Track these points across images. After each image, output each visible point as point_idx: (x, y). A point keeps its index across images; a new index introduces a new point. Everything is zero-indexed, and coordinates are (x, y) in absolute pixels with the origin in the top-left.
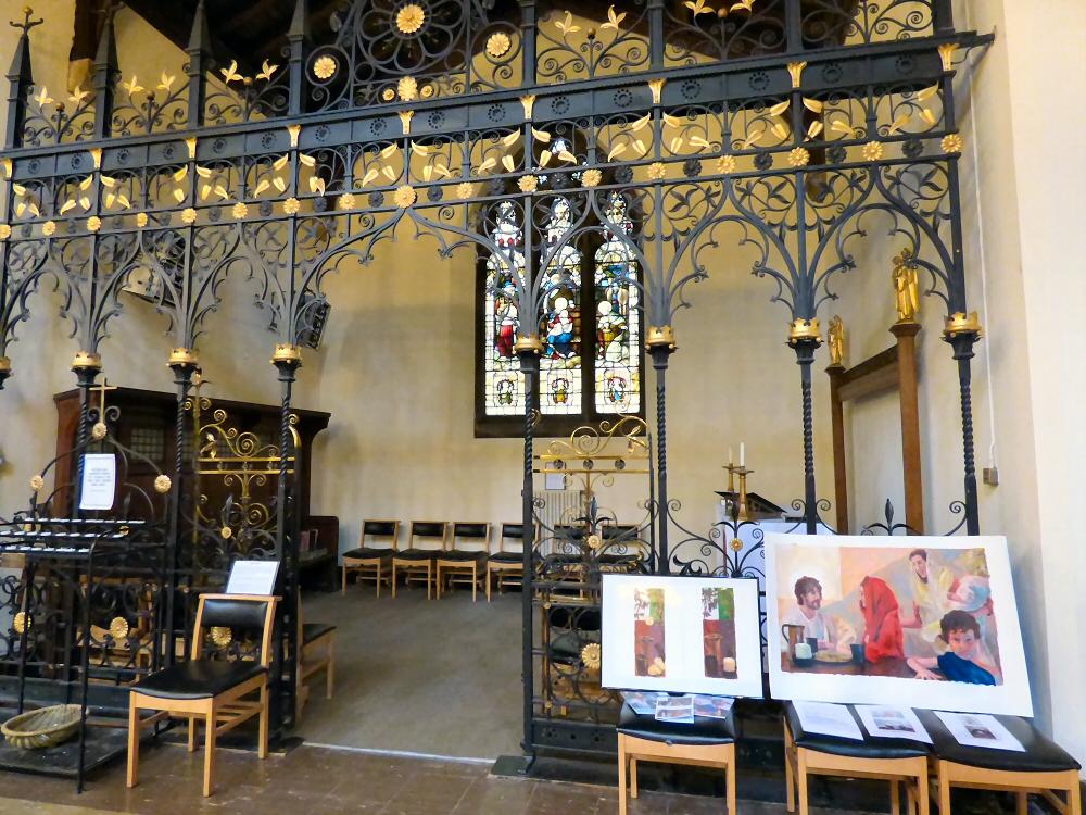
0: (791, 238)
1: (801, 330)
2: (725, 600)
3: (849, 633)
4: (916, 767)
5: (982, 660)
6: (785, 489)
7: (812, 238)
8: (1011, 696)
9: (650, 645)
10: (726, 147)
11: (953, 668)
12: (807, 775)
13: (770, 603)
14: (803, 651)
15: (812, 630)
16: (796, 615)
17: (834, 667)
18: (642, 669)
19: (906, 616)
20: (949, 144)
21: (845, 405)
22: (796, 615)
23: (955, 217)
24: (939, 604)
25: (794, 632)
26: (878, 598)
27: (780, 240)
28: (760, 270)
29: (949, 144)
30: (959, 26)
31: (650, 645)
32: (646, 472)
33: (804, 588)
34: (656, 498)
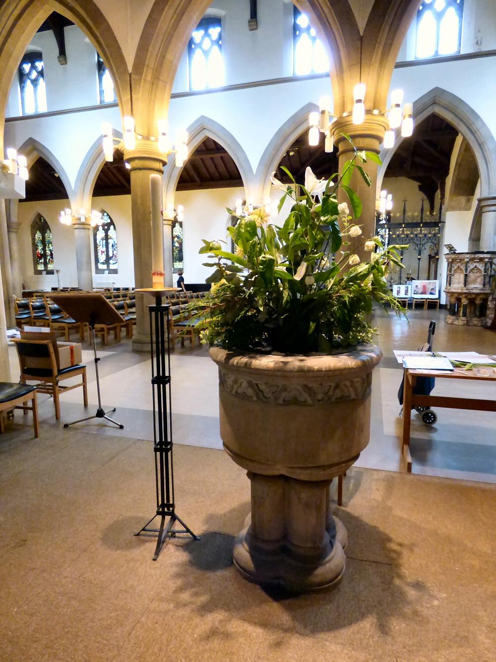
0: (419, 246)
1: (419, 257)
2: (407, 287)
3: (420, 291)
4: (425, 300)
5: (434, 293)
6: (415, 276)
7: (421, 246)
8: (436, 296)
9: (398, 292)
10: (412, 233)
11: (431, 294)
12: (68, 198)
13: (412, 288)
14: (416, 292)
15: (417, 290)
16: (415, 289)
17: (419, 294)
18: (398, 295)
19: (427, 288)
20: (439, 235)
21: (431, 262)
22: (415, 289)
23: (438, 244)
24: (431, 287)
25: (415, 291)
26: (424, 287)
27: (418, 246)
28: (415, 249)
29: (439, 235)
30: (442, 221)
31: (398, 292)
32: (152, 441)
33: (416, 286)
34: (157, 409)
